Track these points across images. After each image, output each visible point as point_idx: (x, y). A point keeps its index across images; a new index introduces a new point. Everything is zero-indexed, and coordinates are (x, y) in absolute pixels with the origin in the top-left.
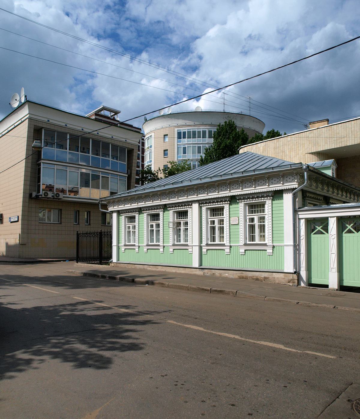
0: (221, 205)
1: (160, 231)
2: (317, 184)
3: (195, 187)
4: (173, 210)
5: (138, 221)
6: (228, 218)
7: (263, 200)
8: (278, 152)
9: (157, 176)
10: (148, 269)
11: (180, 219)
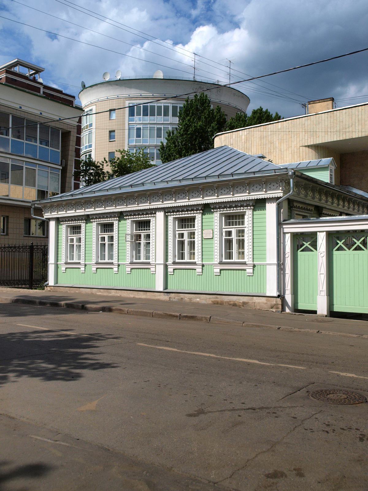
0: (192, 215)
1: (114, 245)
2: (306, 192)
3: (161, 192)
4: (131, 219)
5: (84, 232)
6: (200, 230)
7: (243, 210)
8: (265, 143)
9: (102, 169)
10: (97, 294)
11: (139, 230)
